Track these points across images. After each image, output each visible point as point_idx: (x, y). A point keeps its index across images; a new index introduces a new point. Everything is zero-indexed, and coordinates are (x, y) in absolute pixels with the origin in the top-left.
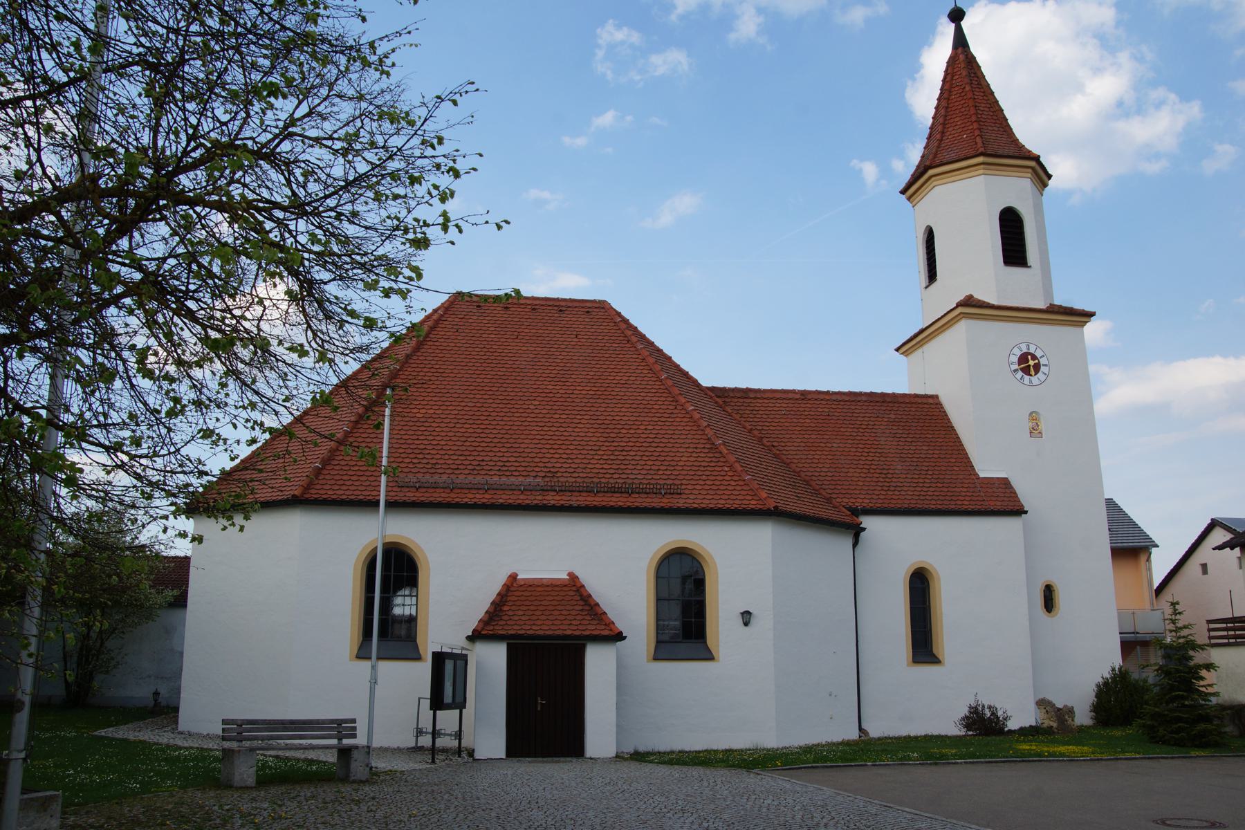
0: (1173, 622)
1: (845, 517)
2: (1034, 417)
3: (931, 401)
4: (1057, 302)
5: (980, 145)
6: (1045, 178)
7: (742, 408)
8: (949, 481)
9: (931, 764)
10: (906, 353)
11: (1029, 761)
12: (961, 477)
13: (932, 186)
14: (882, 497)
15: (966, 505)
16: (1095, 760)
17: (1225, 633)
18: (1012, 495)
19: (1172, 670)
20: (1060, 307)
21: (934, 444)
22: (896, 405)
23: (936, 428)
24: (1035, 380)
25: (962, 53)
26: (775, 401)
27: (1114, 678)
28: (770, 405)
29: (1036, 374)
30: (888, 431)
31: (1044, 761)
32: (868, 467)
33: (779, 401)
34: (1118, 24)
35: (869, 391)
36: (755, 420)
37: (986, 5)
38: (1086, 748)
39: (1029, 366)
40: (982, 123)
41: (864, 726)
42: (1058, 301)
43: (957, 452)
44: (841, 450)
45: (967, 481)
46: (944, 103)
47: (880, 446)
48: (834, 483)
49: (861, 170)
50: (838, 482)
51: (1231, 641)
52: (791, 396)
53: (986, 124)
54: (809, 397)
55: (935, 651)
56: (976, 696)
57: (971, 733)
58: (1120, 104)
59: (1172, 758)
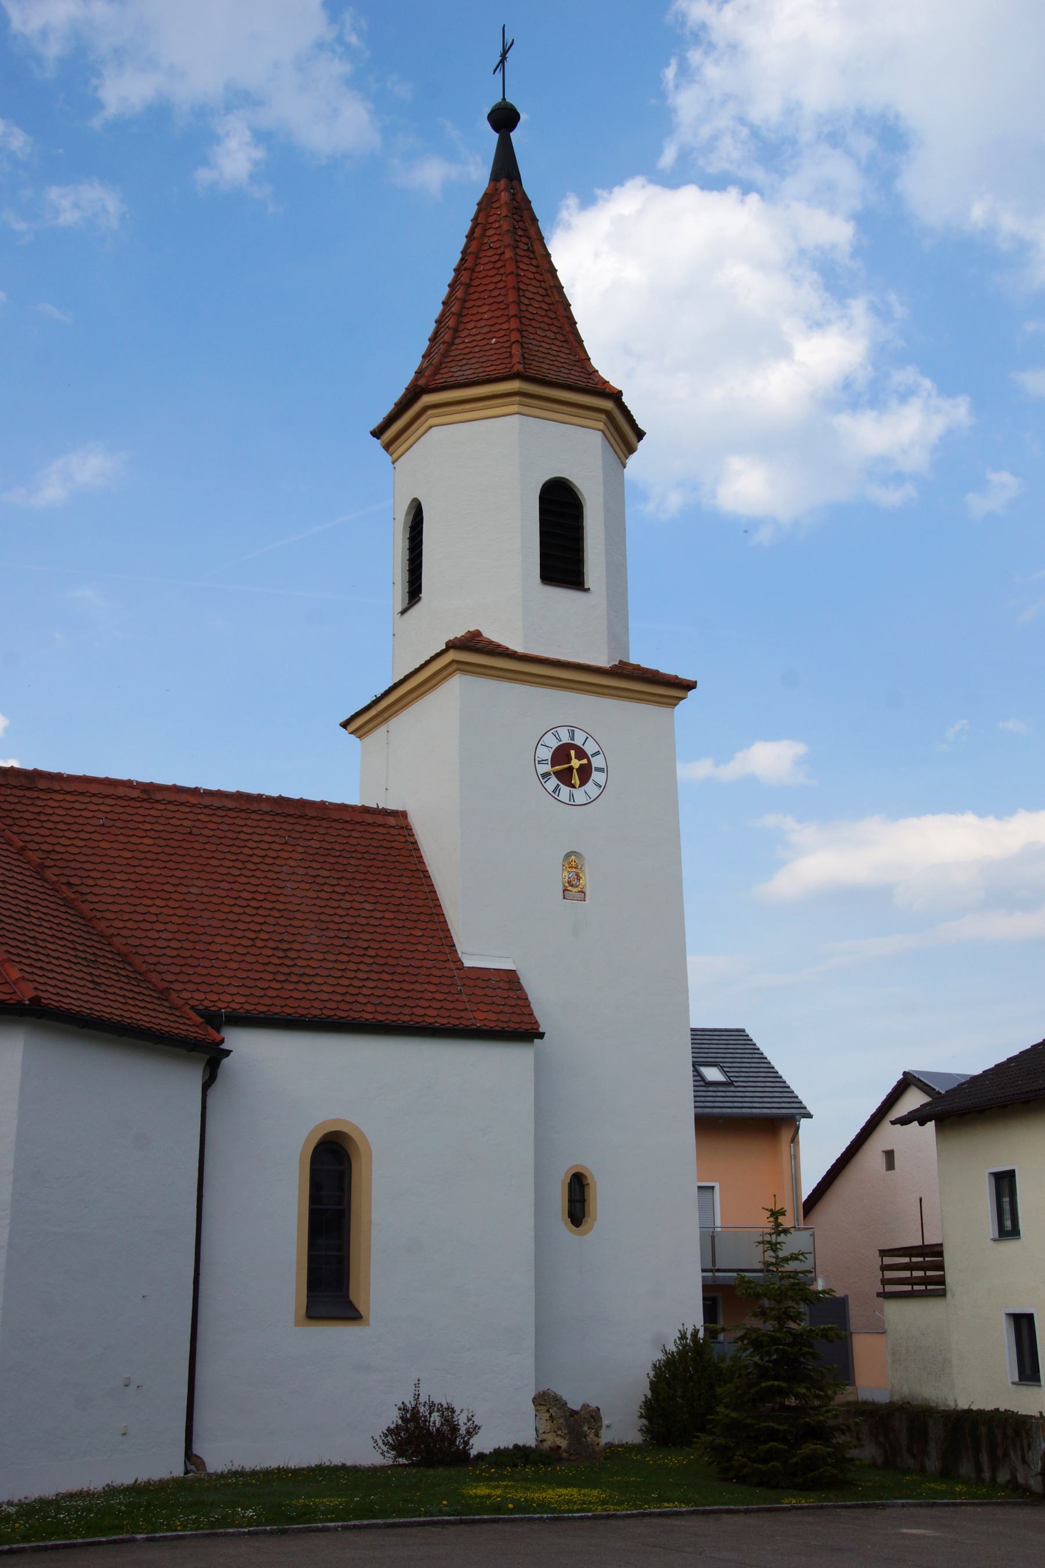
0: (774, 1247)
1: (193, 1028)
2: (572, 861)
3: (392, 821)
4: (634, 660)
5: (516, 359)
6: (631, 436)
7: (19, 807)
8: (406, 970)
9: (272, 1532)
10: (360, 733)
11: (474, 1522)
12: (430, 964)
14: (271, 993)
15: (432, 1017)
16: (602, 1517)
17: (906, 1274)
18: (521, 1003)
19: (765, 1339)
20: (637, 667)
21: (386, 900)
22: (324, 824)
23: (395, 872)
24: (579, 795)
25: (506, 189)
26: (87, 800)
27: (682, 1353)
28: (77, 805)
29: (582, 784)
30: (301, 871)
31: (504, 1521)
32: (253, 935)
33: (95, 800)
34: (857, 252)
35: (275, 794)
36: (42, 832)
37: (643, 186)
38: (595, 1492)
39: (571, 769)
40: (527, 322)
41: (197, 1450)
42: (640, 657)
43: (427, 918)
44: (206, 899)
45: (439, 973)
46: (465, 278)
47: (282, 899)
48: (182, 961)
50: (190, 961)
51: (916, 1288)
52: (120, 791)
53: (533, 323)
54: (158, 797)
55: (353, 1297)
56: (417, 1385)
57: (402, 1461)
58: (847, 385)
59: (747, 1511)
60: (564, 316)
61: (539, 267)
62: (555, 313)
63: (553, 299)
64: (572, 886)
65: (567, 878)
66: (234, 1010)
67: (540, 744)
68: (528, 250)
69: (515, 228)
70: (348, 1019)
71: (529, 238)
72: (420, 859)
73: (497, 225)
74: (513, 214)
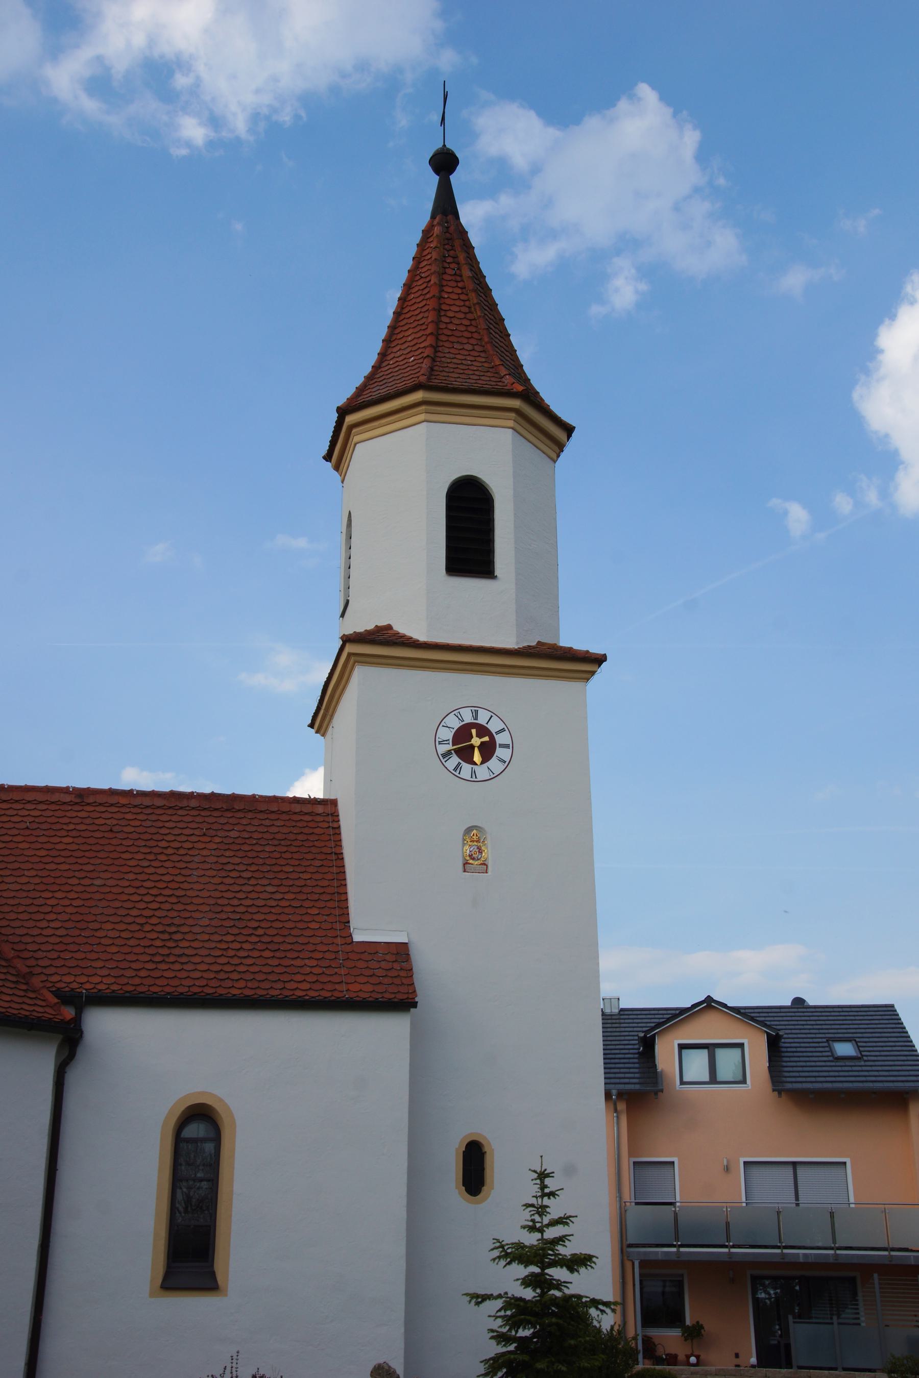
0: (542, 1210)
13: (353, 445)
22: (250, 815)
24: (482, 772)
39: (472, 747)
49: (786, 513)
54: (91, 799)
60: (484, 329)
61: (465, 288)
62: (477, 327)
63: (475, 315)
64: (474, 859)
65: (468, 852)
66: (100, 990)
67: (441, 725)
68: (455, 274)
69: (445, 257)
70: (228, 995)
71: (458, 264)
72: (338, 843)
73: (429, 257)
74: (445, 245)
